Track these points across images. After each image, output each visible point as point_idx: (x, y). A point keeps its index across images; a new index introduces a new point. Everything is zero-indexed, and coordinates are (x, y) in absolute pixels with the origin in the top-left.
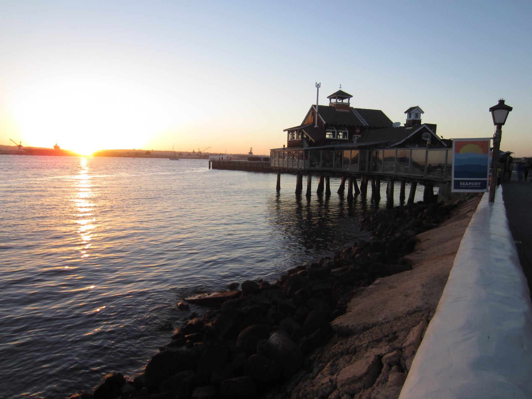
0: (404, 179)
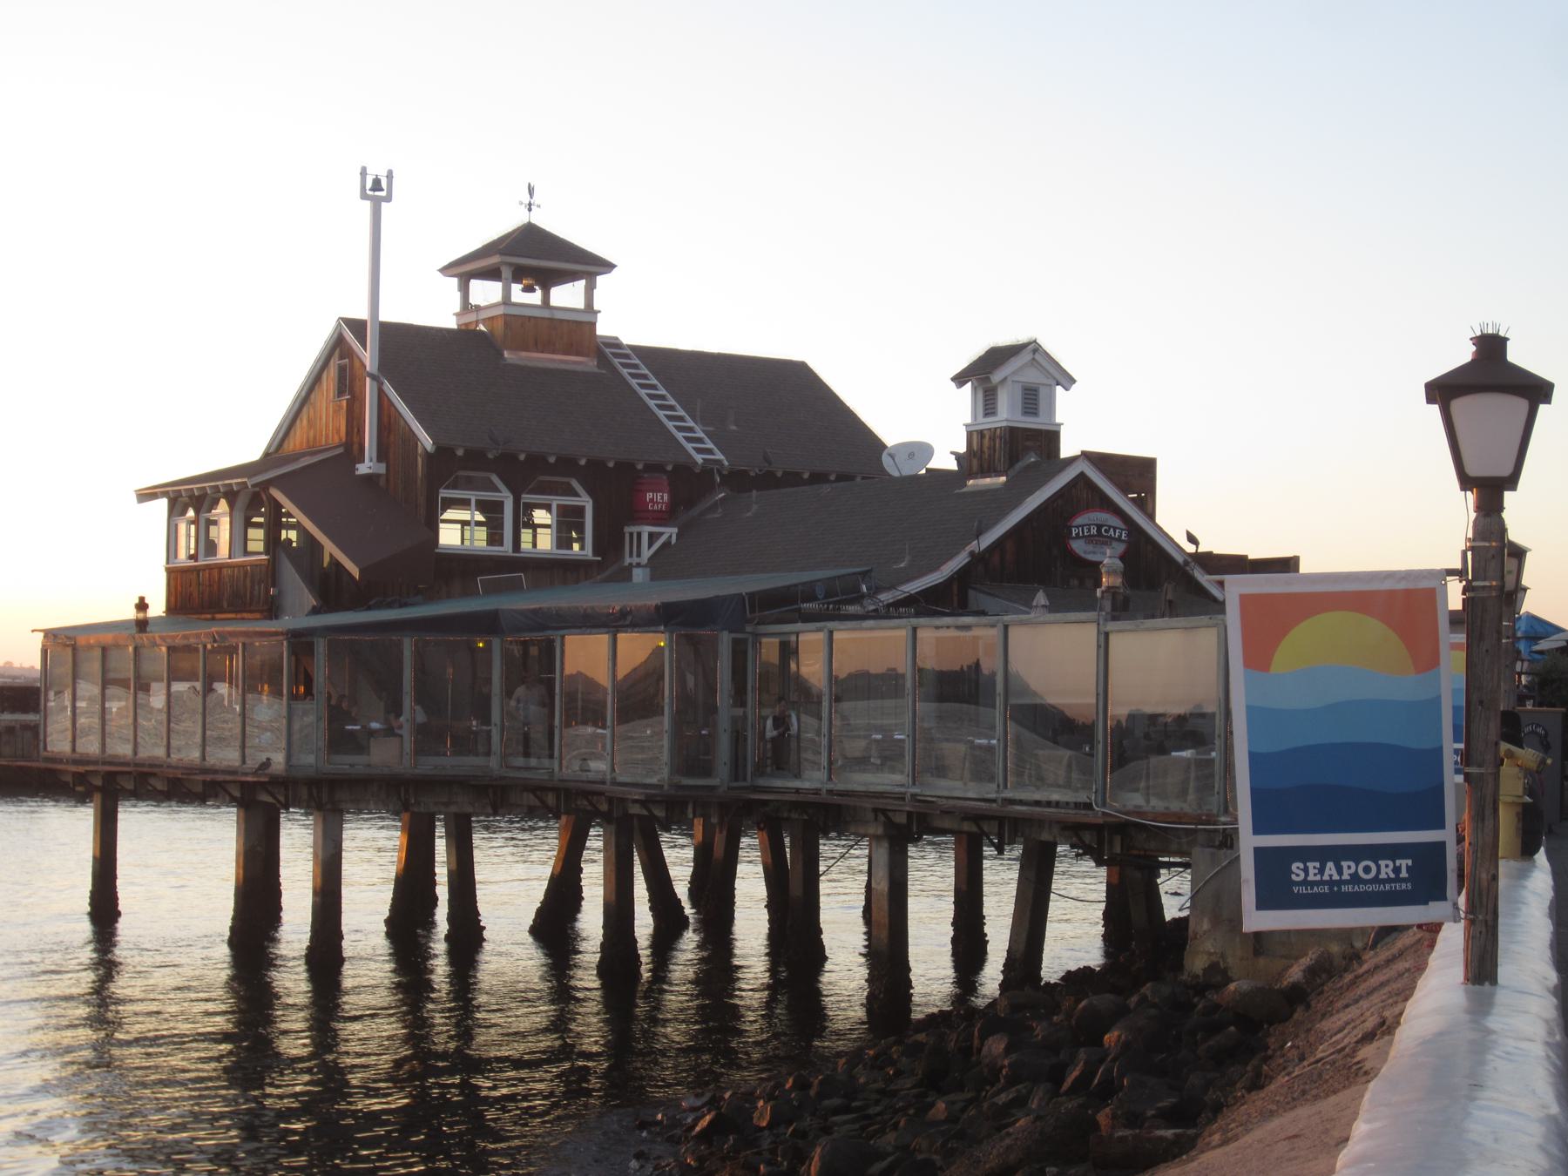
0: (968, 827)
